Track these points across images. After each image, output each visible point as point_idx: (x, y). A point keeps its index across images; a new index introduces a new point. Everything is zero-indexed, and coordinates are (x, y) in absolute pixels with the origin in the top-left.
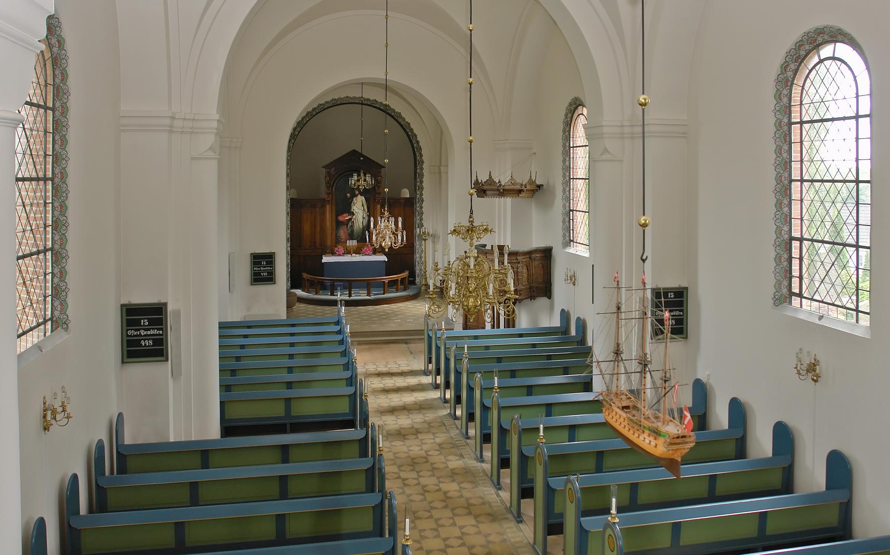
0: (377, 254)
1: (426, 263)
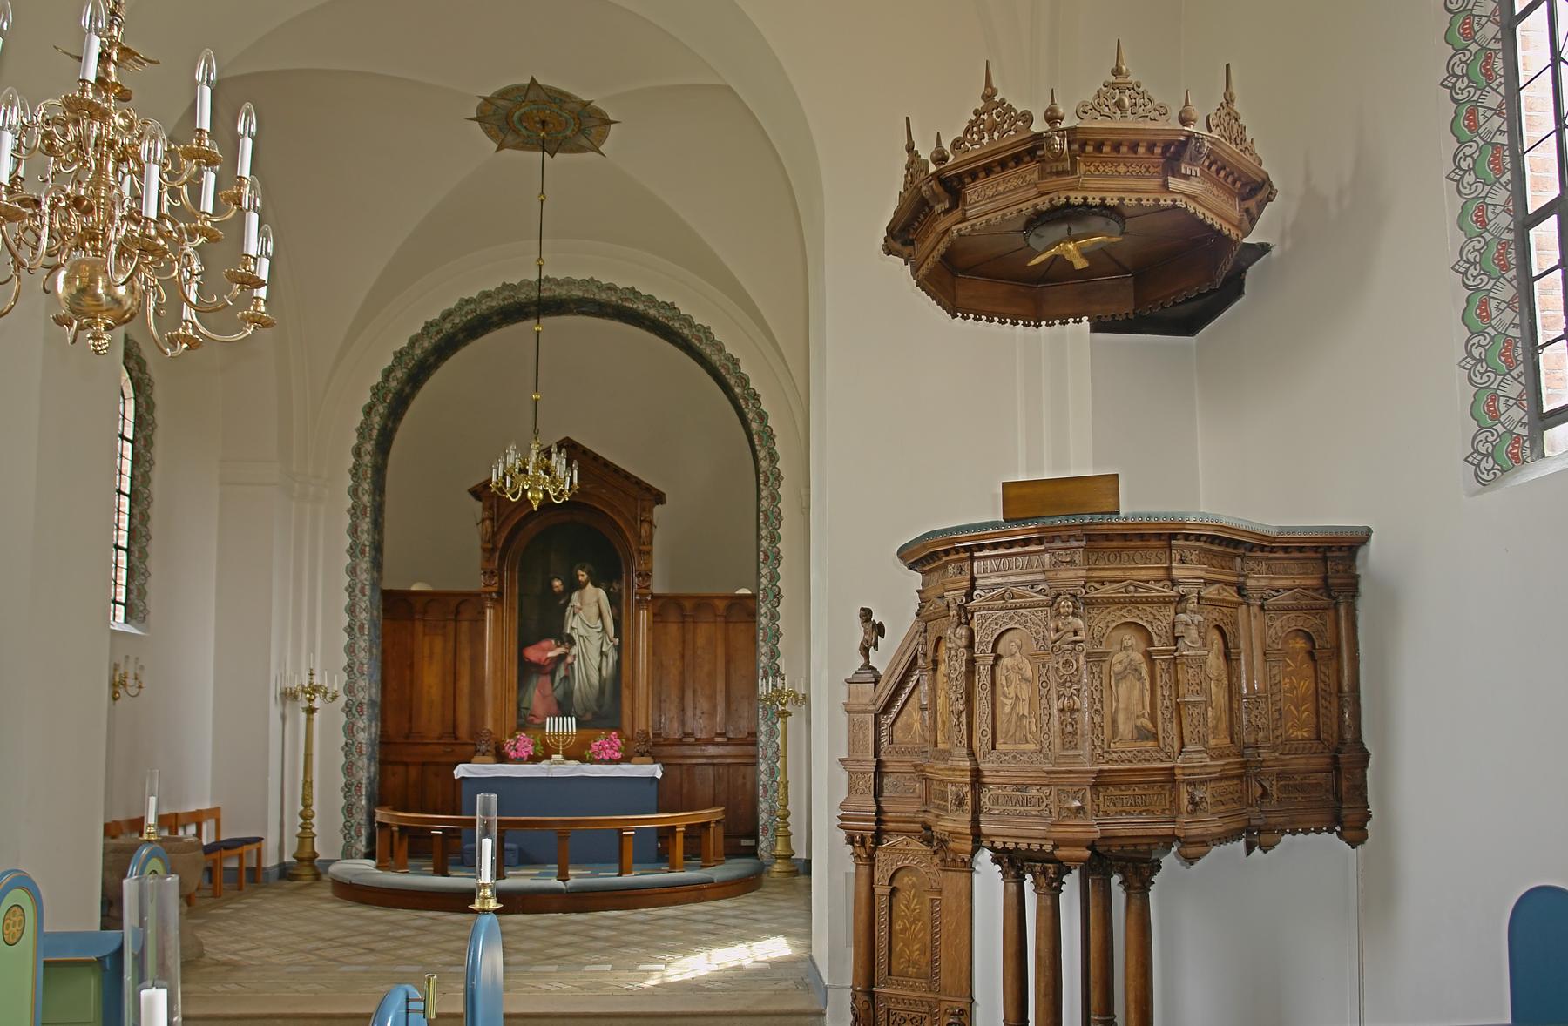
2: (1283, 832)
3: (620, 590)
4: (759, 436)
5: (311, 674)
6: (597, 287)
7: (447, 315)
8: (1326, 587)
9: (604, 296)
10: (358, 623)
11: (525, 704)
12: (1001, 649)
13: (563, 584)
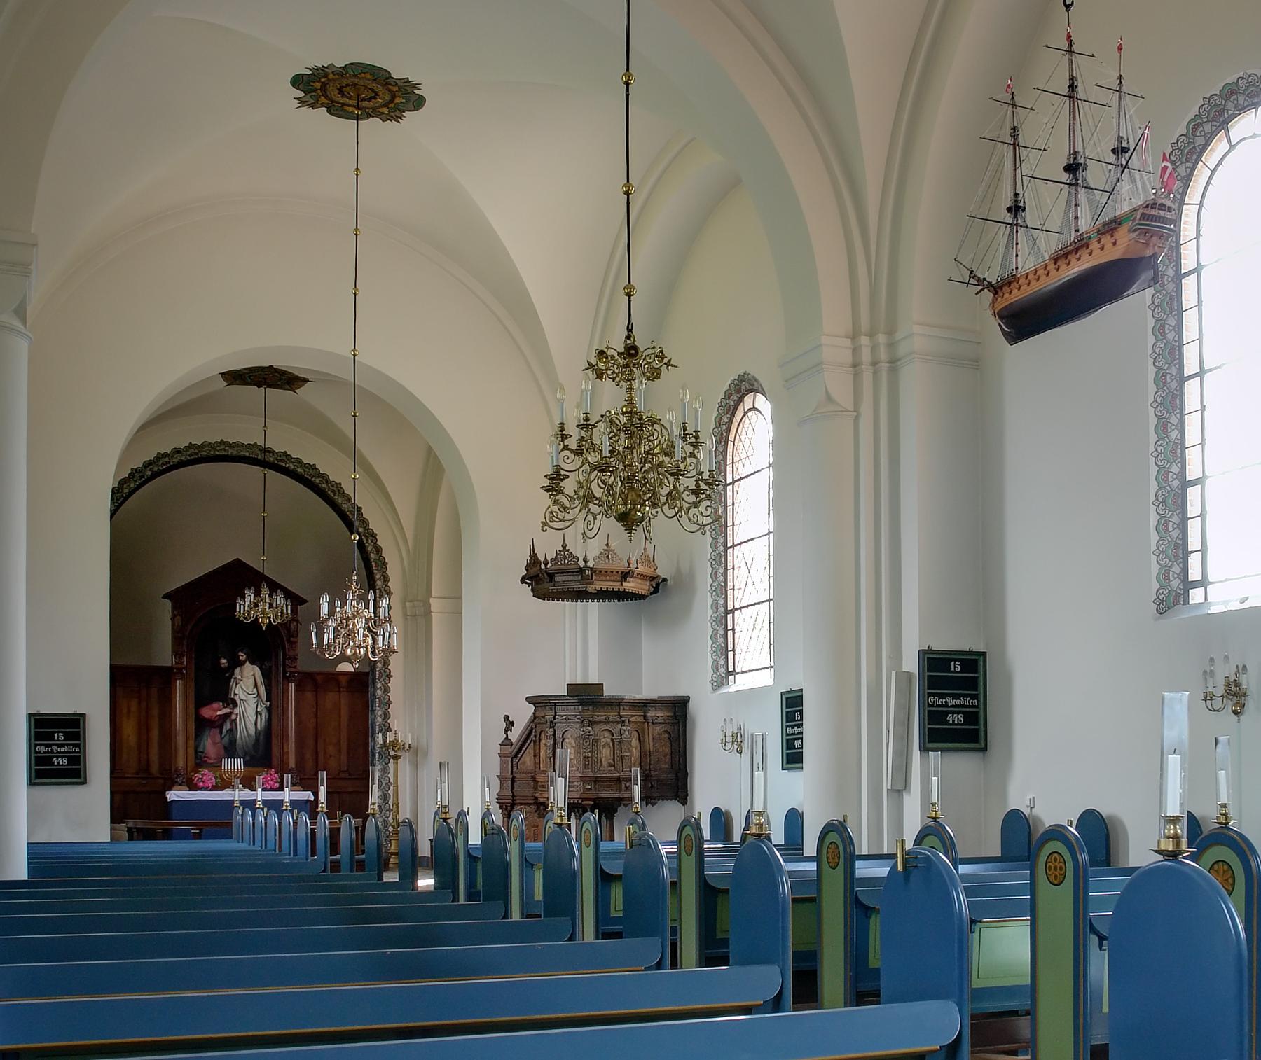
1: (398, 807)
2: (659, 800)
3: (271, 667)
4: (376, 563)
8: (675, 716)
11: (201, 749)
12: (564, 737)
13: (228, 661)
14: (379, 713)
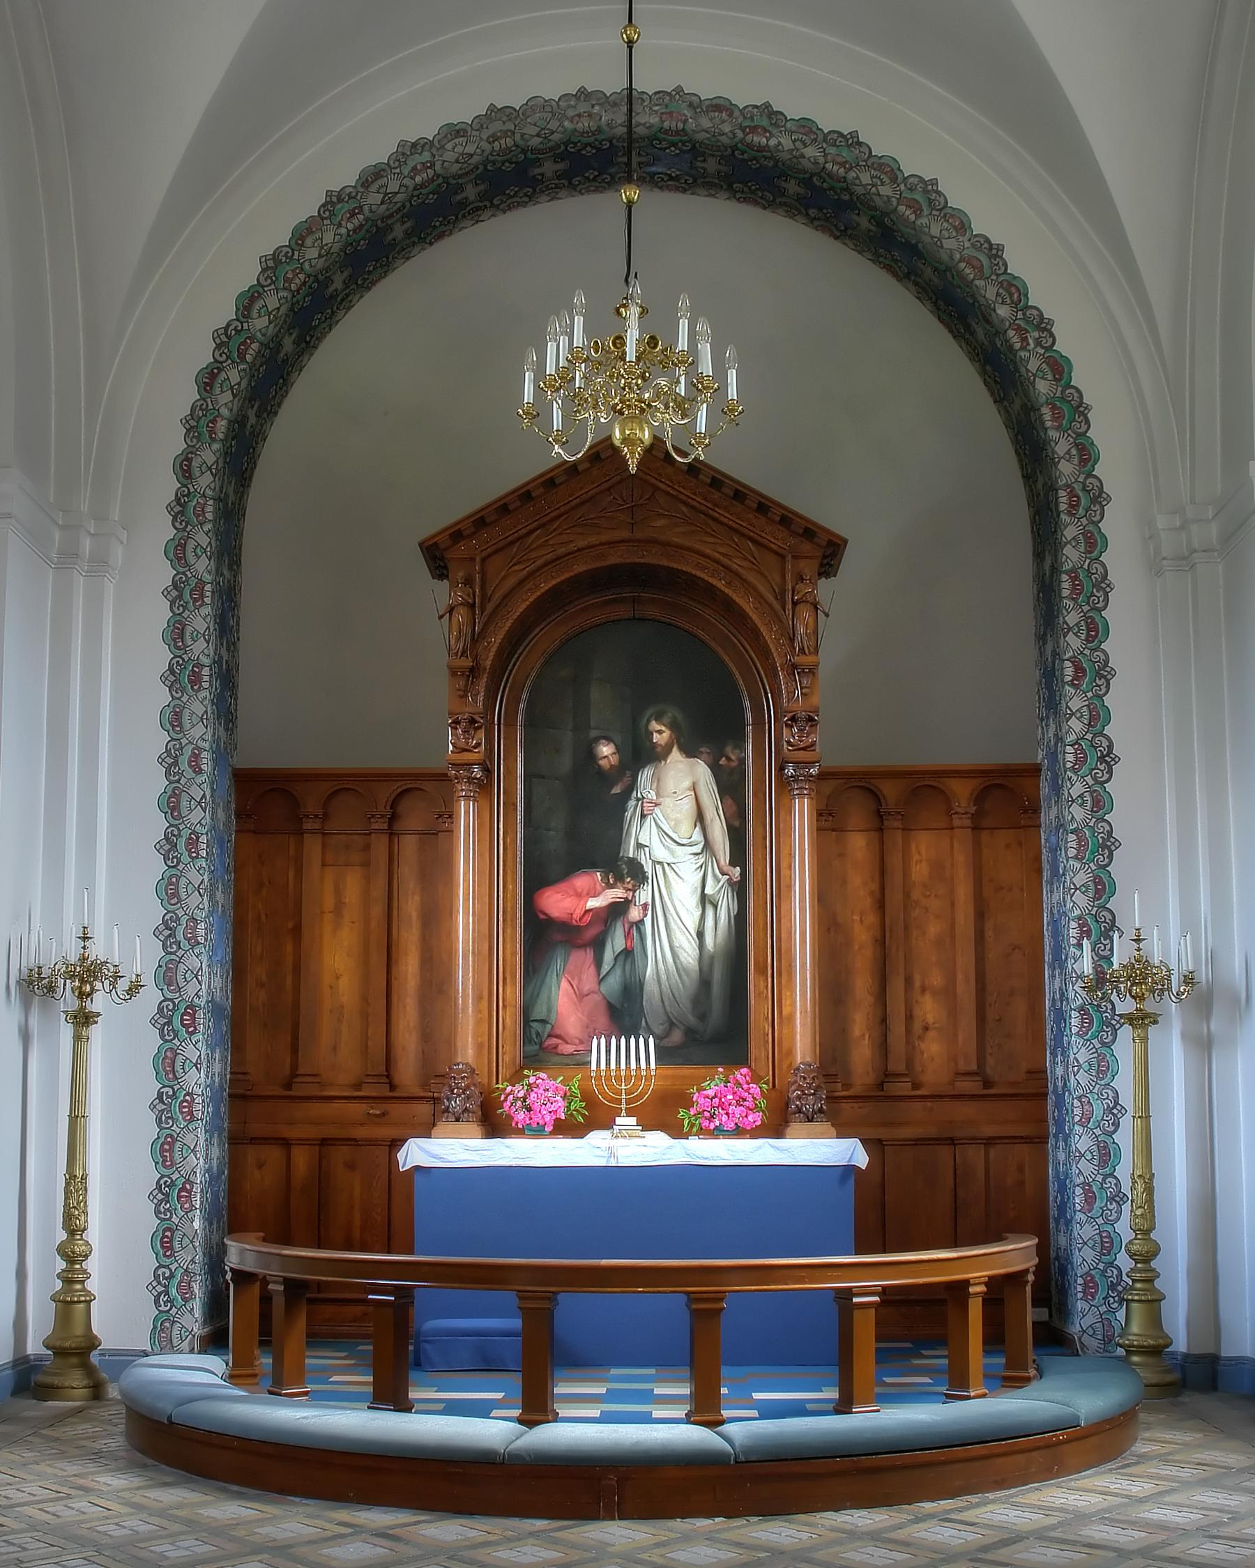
0: (794, 1127)
3: (742, 762)
4: (1054, 408)
5: (85, 938)
6: (691, 105)
7: (372, 176)
9: (705, 123)
10: (186, 833)
13: (618, 750)
14: (1076, 790)
